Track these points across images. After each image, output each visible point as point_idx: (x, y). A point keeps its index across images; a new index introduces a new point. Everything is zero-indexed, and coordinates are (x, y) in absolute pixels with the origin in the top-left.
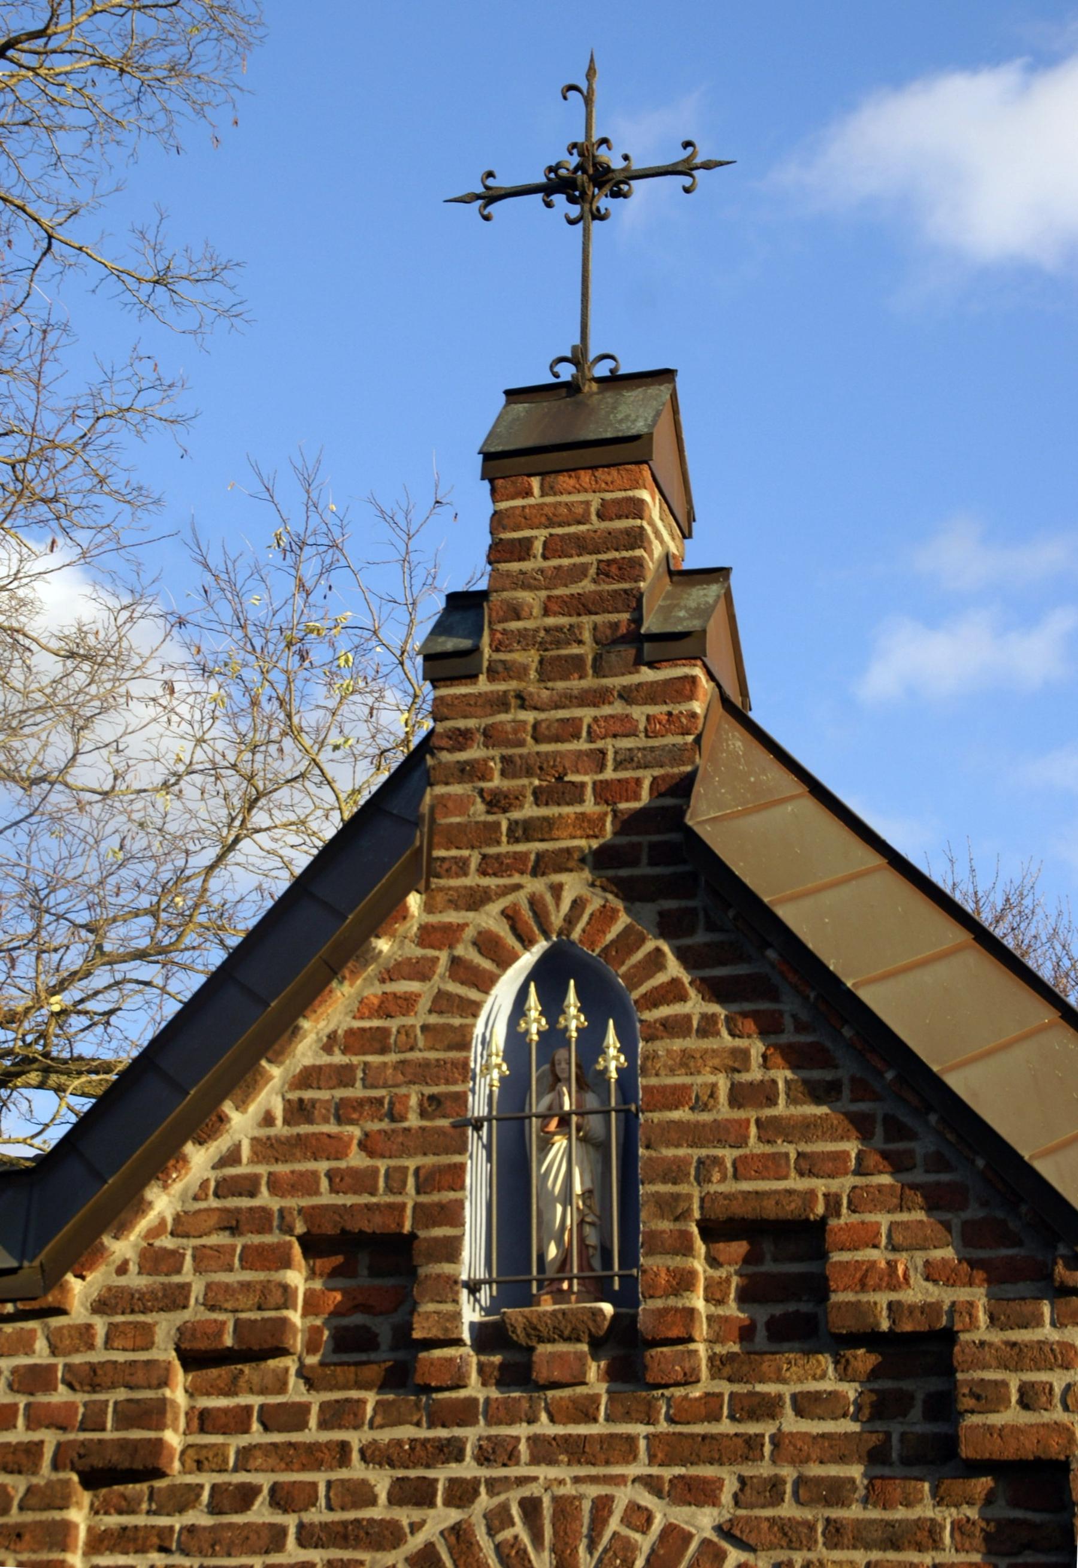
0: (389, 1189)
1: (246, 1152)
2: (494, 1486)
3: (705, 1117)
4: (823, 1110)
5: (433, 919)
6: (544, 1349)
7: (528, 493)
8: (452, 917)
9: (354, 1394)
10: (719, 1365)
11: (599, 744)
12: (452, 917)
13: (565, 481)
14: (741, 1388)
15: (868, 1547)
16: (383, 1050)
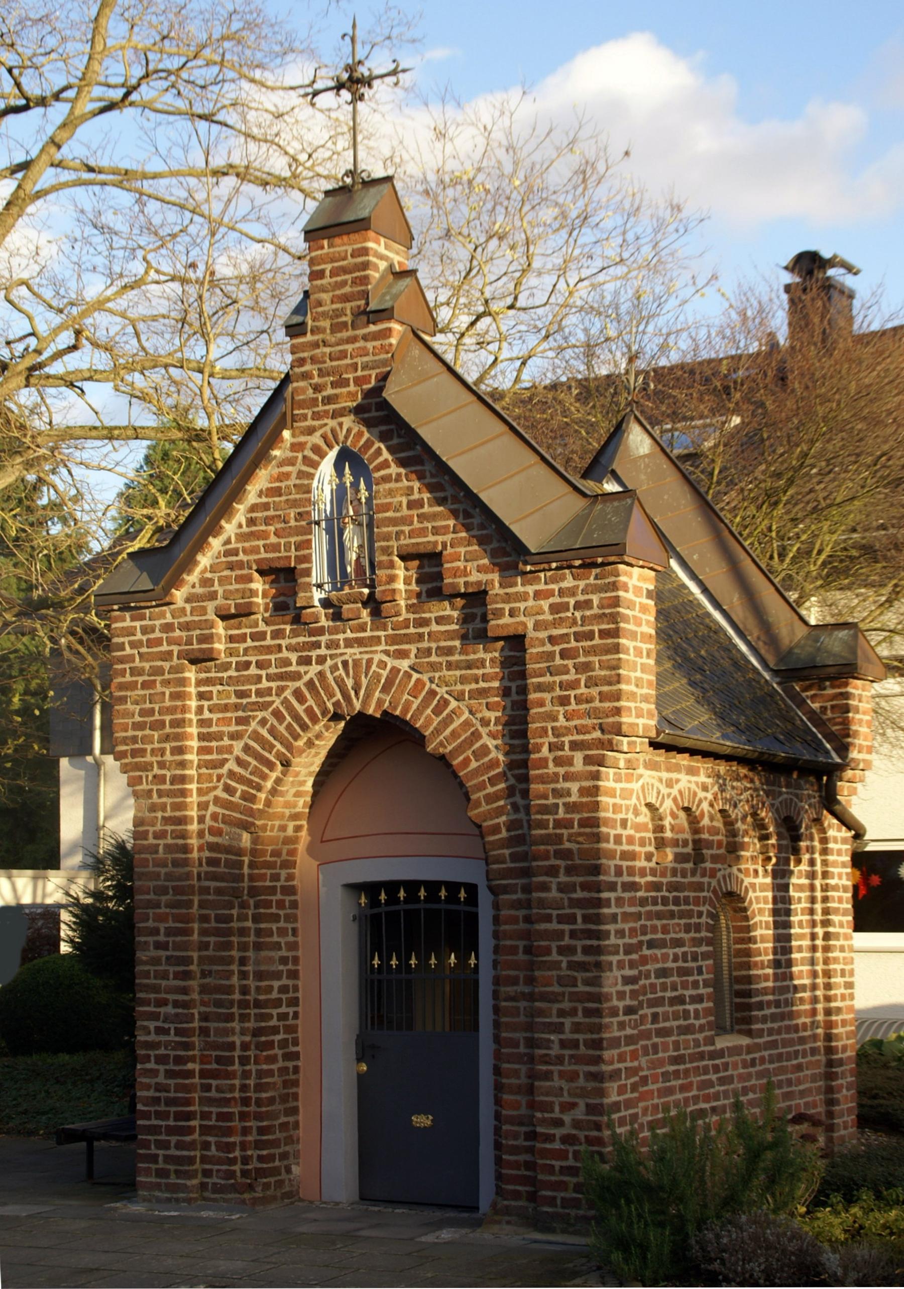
0: (285, 550)
1: (233, 539)
2: (332, 657)
3: (398, 515)
4: (441, 509)
5: (295, 440)
6: (345, 607)
7: (322, 248)
8: (302, 439)
9: (282, 627)
10: (409, 608)
11: (355, 360)
12: (302, 439)
13: (337, 241)
14: (417, 616)
15: (461, 669)
16: (280, 495)
